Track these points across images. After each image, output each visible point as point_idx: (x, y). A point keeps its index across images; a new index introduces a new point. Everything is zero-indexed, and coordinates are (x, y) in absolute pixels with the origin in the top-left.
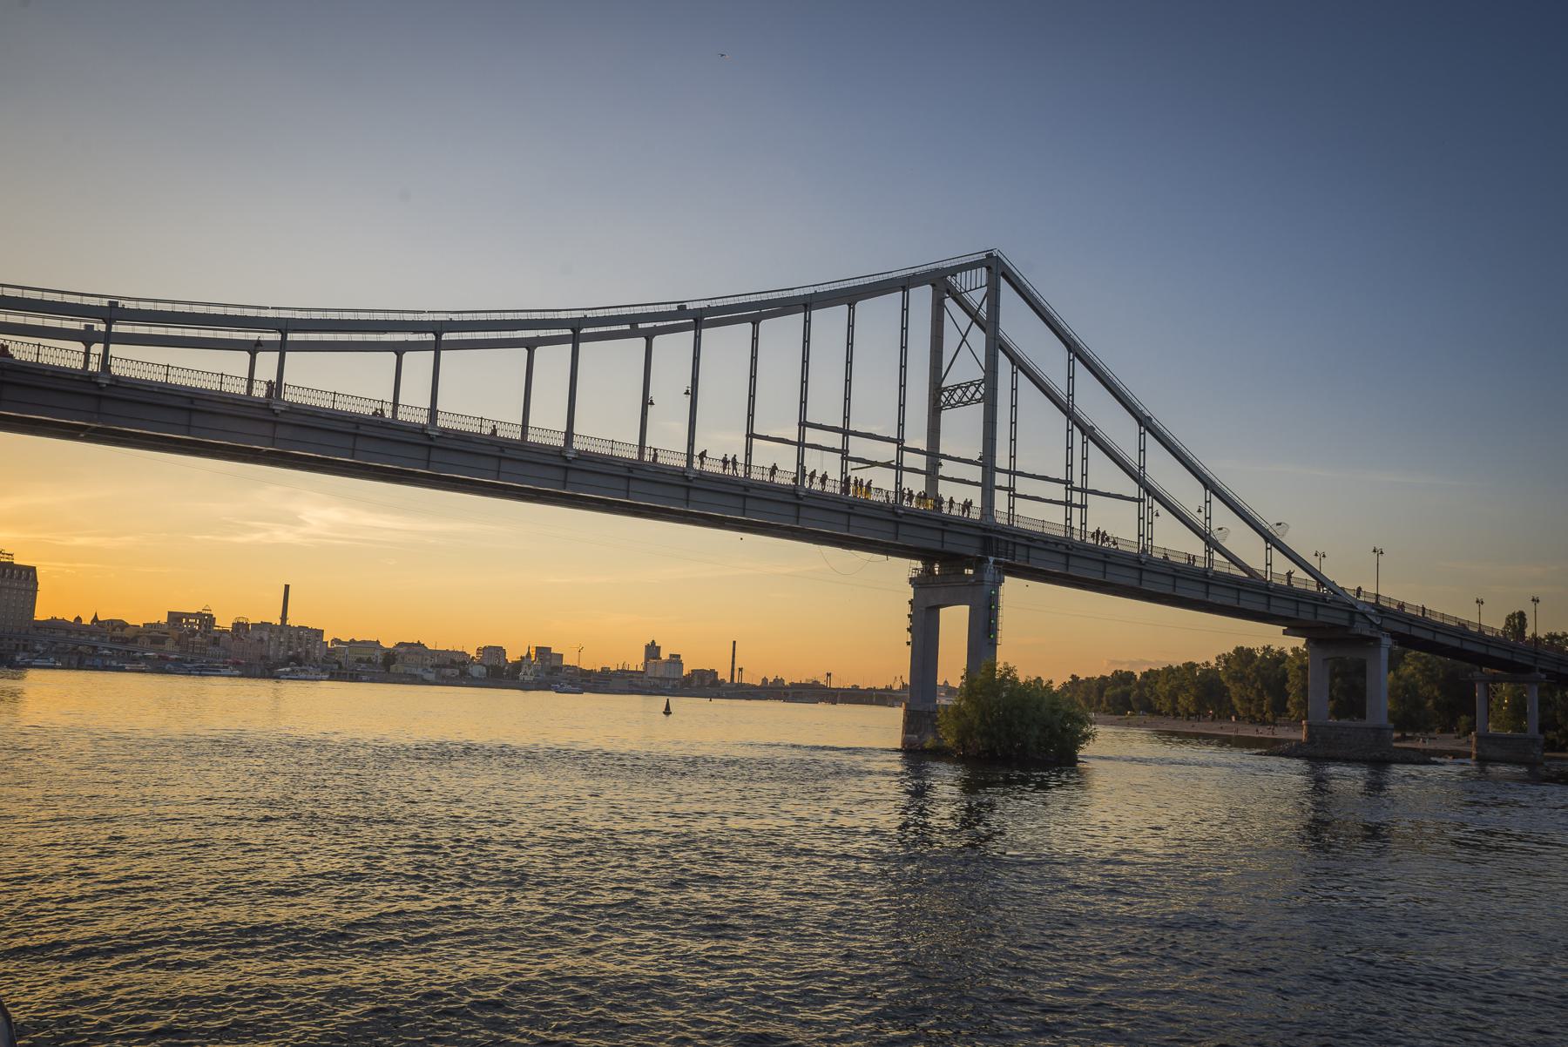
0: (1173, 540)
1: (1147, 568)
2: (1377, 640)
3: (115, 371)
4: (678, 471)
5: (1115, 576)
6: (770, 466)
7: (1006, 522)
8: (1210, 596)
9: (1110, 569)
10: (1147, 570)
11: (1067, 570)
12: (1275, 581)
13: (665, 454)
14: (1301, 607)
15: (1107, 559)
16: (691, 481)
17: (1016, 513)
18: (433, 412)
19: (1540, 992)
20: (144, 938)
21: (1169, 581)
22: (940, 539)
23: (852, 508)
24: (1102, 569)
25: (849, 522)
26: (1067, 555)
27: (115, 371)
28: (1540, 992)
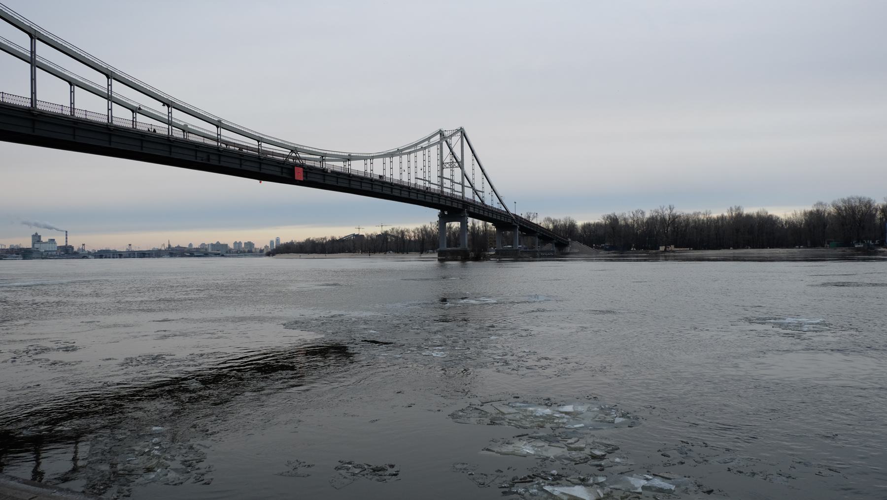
0: (122, 117)
1: (174, 144)
2: (517, 226)
3: (76, 115)
4: (104, 125)
5: (247, 166)
6: (668, 206)
7: (69, 113)
8: (262, 170)
9: (223, 159)
10: (175, 146)
11: (110, 145)
12: (352, 173)
13: (117, 119)
14: (434, 198)
15: (242, 158)
16: (112, 131)
17: (137, 121)
18: (72, 109)
19: (718, 423)
20: (60, 405)
21: (238, 161)
22: (239, 163)
23: (198, 148)
24: (390, 190)
25: (196, 155)
26: (241, 159)
27: (76, 115)
28: (718, 423)
